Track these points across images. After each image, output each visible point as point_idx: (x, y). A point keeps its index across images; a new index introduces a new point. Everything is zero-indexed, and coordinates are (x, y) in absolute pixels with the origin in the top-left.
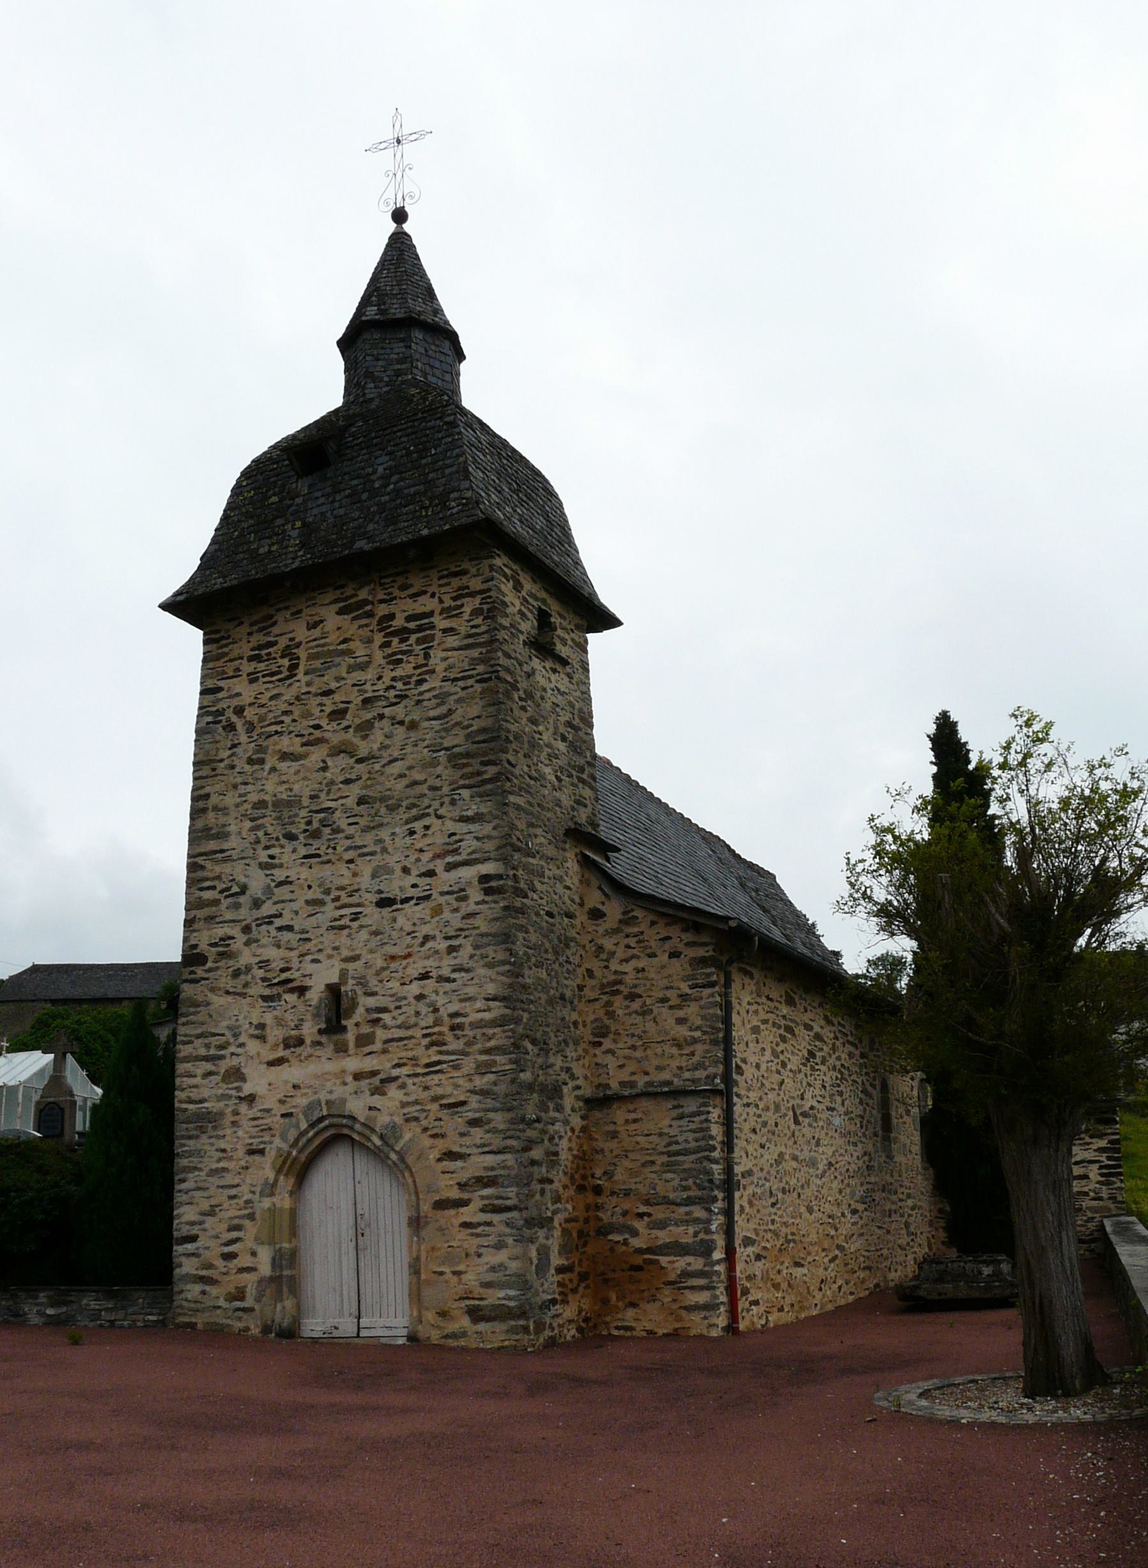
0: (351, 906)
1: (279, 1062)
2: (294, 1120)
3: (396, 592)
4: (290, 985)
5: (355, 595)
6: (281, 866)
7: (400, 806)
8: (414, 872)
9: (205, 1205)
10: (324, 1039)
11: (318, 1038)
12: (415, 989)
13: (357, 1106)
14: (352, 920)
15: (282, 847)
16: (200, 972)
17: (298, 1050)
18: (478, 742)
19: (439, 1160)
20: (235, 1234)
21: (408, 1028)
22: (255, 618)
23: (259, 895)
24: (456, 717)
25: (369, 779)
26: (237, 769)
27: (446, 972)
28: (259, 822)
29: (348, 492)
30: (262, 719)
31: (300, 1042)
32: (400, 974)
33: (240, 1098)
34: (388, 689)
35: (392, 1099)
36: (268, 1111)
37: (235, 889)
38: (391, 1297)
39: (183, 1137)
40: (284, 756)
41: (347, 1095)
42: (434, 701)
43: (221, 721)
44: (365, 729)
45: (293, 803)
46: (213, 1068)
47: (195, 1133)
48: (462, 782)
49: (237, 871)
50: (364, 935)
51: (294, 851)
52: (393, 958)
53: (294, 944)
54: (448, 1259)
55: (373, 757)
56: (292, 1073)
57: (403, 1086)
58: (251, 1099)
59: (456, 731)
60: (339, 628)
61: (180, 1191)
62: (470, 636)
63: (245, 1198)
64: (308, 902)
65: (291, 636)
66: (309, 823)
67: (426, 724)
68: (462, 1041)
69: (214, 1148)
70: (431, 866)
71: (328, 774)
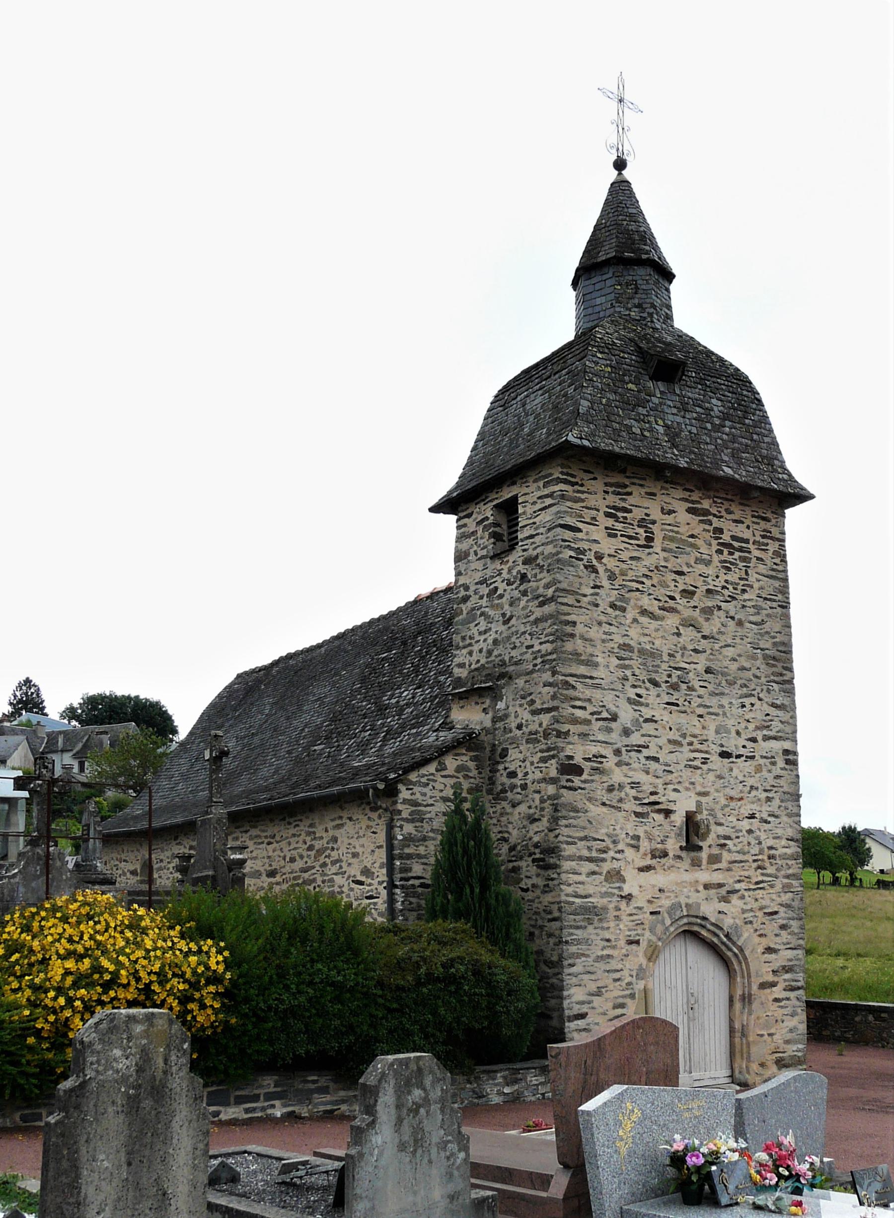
0: (701, 751)
1: (648, 868)
2: (660, 917)
3: (724, 513)
4: (657, 807)
5: (699, 503)
6: (647, 705)
7: (735, 683)
8: (744, 736)
9: (593, 987)
10: (684, 854)
11: (679, 853)
12: (746, 824)
13: (709, 909)
14: (702, 763)
15: (647, 689)
16: (577, 781)
17: (663, 860)
18: (781, 651)
19: (763, 953)
20: (619, 1011)
21: (744, 854)
22: (608, 480)
23: (629, 725)
24: (767, 627)
25: (711, 654)
26: (601, 609)
27: (765, 816)
28: (627, 662)
29: (695, 415)
30: (623, 573)
31: (665, 854)
32: (736, 812)
33: (622, 897)
34: (724, 587)
35: (735, 906)
36: (640, 908)
37: (605, 715)
38: (713, 1055)
39: (571, 927)
40: (644, 612)
41: (700, 901)
42: (752, 610)
43: (582, 560)
44: (708, 612)
45: (654, 654)
46: (597, 869)
47: (583, 924)
48: (772, 677)
49: (608, 699)
50: (711, 777)
51: (658, 696)
52: (731, 798)
53: (660, 773)
54: (766, 1026)
55: (713, 638)
56: (658, 879)
57: (742, 897)
58: (629, 897)
59: (766, 637)
60: (688, 524)
61: (569, 975)
62: (773, 570)
63: (626, 981)
64: (669, 741)
65: (646, 511)
66: (670, 676)
67: (748, 625)
68: (775, 867)
69: (599, 938)
70: (754, 735)
71: (681, 640)
